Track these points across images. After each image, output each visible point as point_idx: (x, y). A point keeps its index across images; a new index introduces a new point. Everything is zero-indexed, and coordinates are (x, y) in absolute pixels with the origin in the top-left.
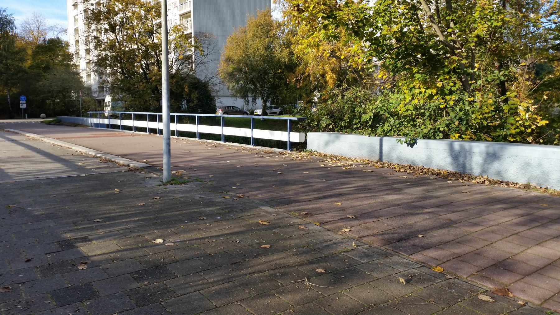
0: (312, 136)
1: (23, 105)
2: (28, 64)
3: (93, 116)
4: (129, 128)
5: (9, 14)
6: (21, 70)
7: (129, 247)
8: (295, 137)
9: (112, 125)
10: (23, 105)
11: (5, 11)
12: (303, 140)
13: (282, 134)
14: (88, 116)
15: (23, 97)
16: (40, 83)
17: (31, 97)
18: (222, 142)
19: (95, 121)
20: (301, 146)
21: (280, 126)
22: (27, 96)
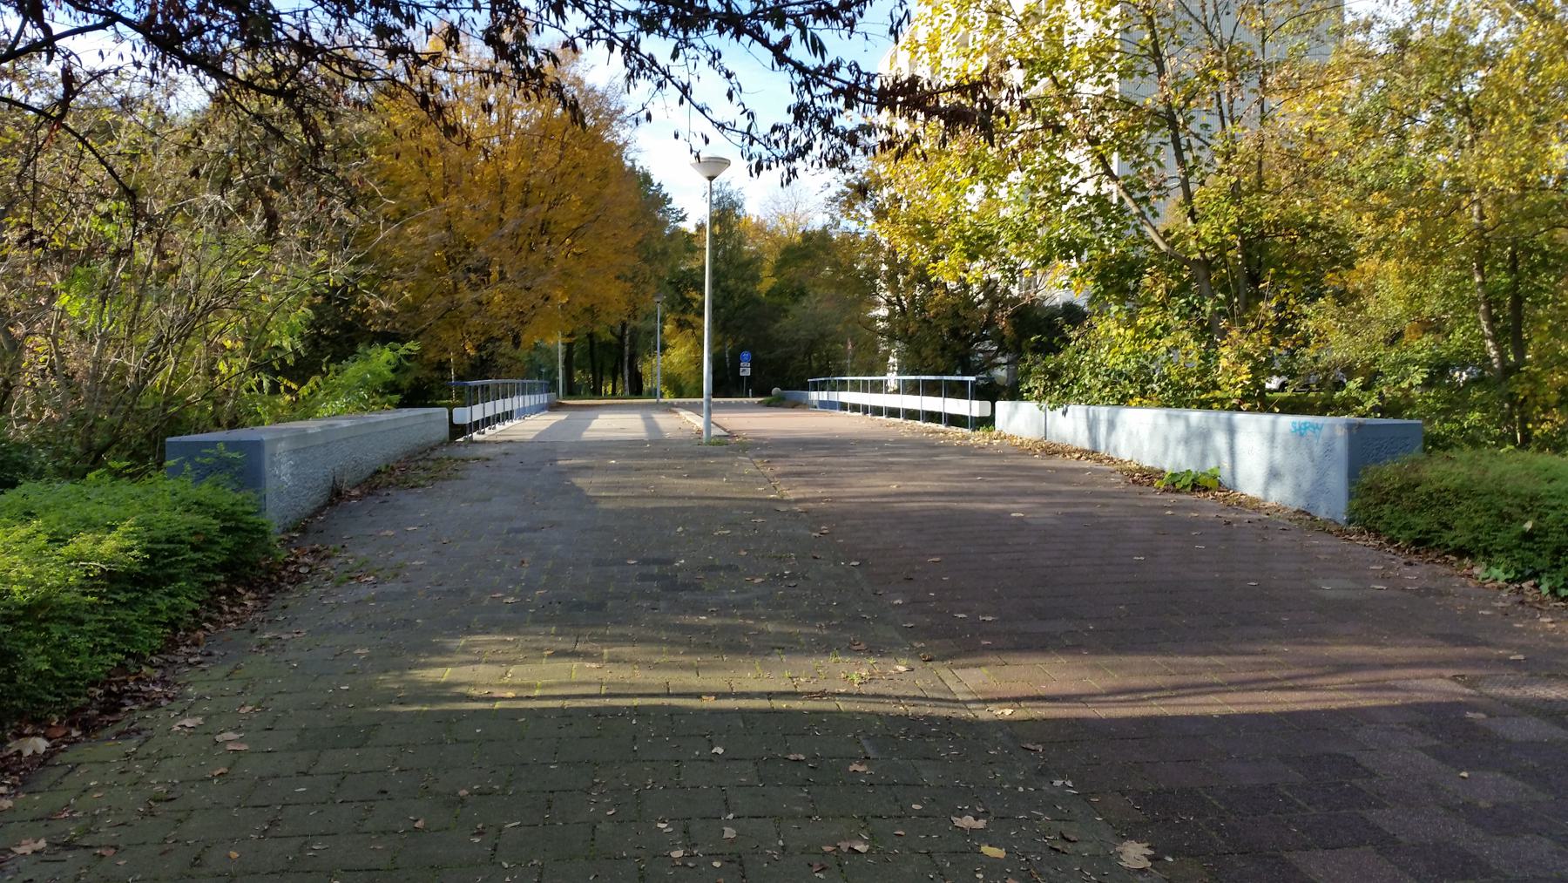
0: (1001, 406)
1: (746, 371)
2: (767, 283)
3: (816, 387)
4: (843, 407)
5: (735, 189)
6: (752, 300)
7: (980, 697)
8: (972, 408)
9: (928, 412)
10: (746, 371)
11: (728, 183)
12: (988, 414)
13: (1016, 407)
14: (806, 387)
15: (746, 355)
16: (778, 325)
17: (760, 354)
18: (942, 427)
19: (824, 396)
20: (987, 422)
21: (957, 391)
22: (753, 352)
